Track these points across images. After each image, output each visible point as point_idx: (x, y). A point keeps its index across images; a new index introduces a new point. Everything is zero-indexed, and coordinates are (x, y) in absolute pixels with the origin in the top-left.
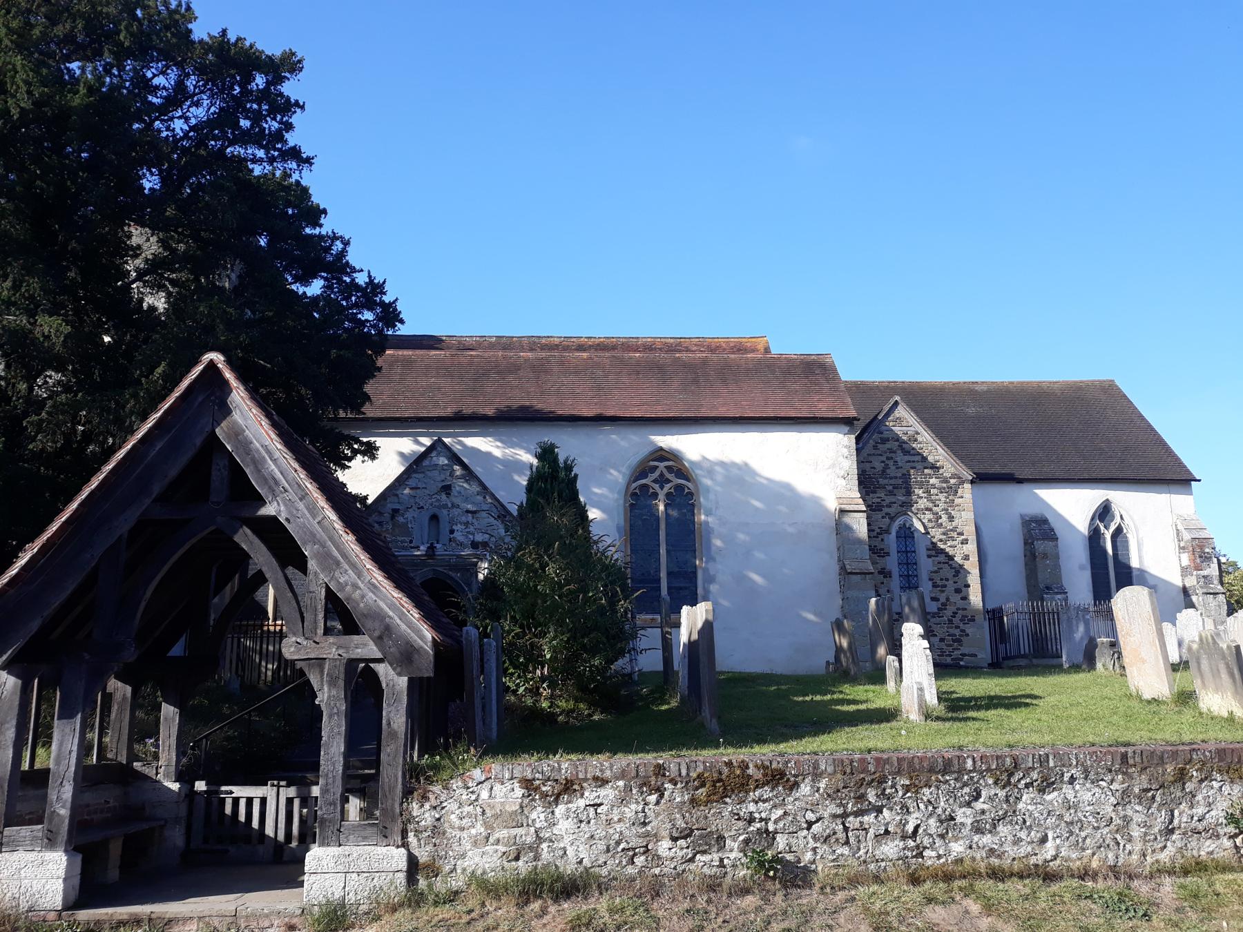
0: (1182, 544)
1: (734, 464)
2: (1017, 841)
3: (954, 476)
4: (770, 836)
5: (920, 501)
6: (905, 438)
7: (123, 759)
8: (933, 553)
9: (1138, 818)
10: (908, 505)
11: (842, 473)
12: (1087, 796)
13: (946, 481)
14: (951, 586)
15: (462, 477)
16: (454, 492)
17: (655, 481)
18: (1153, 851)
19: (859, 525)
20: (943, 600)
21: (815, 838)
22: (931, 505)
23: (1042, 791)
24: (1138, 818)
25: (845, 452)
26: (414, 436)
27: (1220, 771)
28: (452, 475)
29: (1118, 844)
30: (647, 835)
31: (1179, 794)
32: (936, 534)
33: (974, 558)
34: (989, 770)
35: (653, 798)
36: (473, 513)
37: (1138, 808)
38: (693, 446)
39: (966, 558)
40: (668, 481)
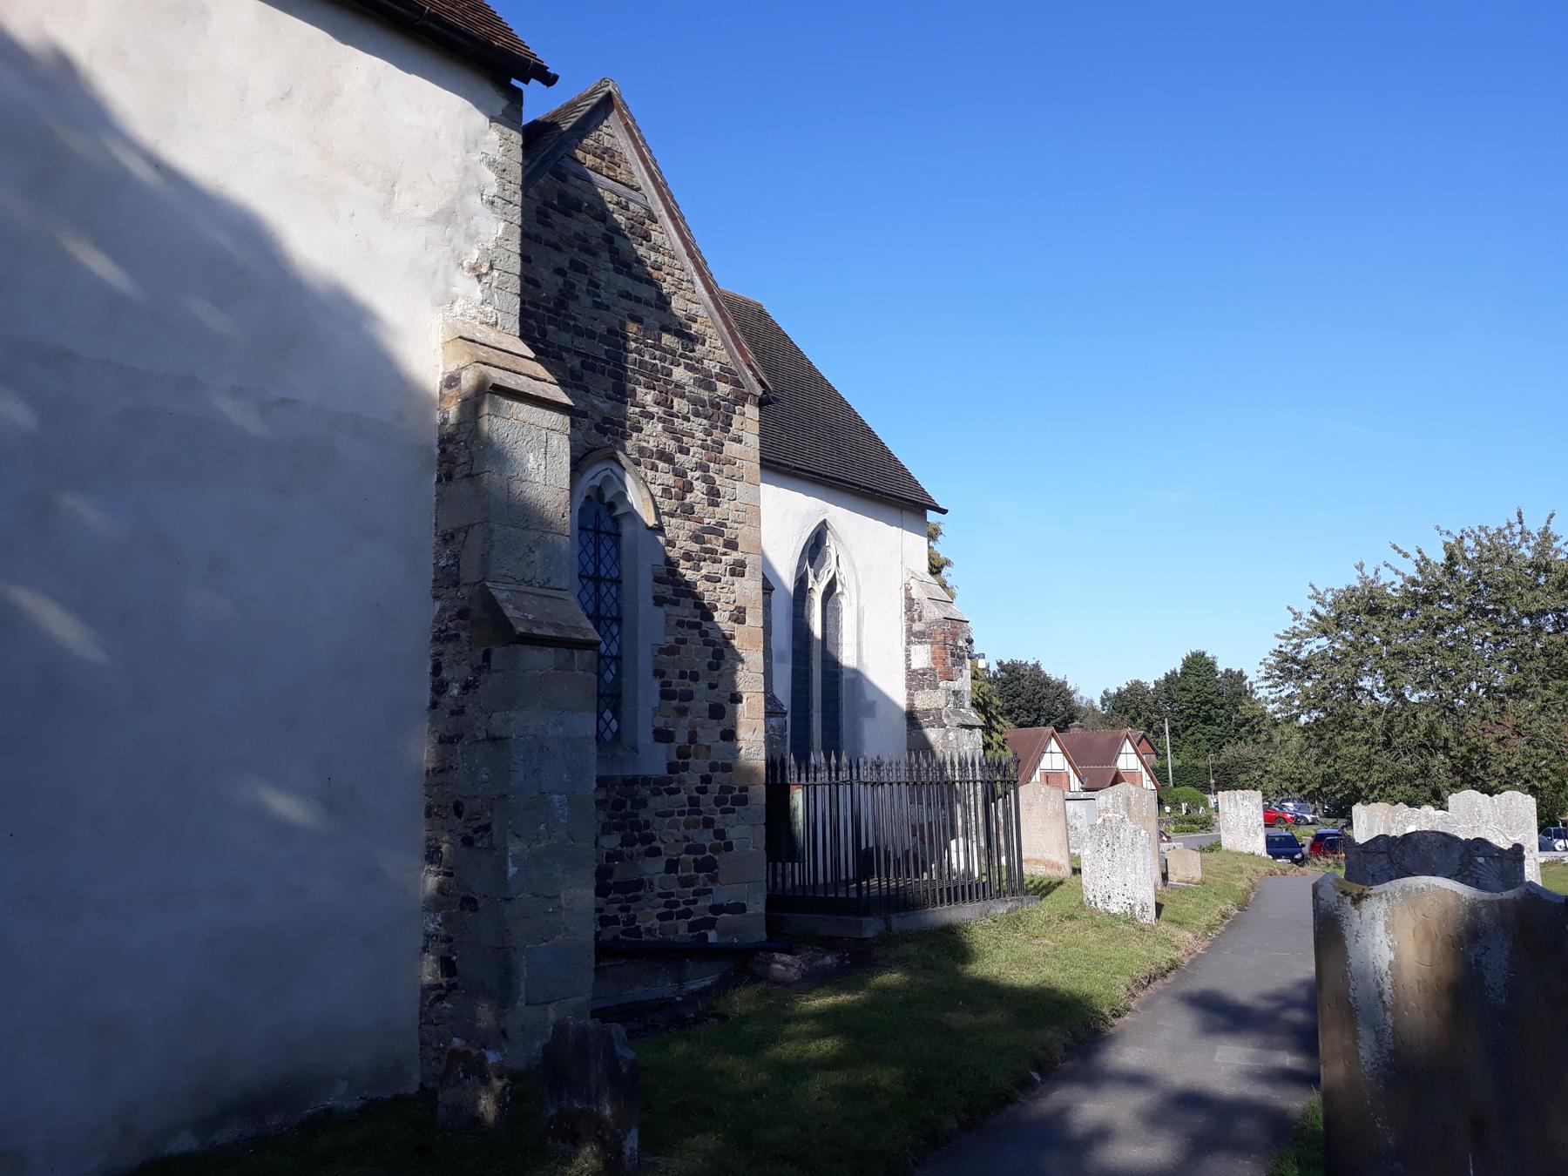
0: (917, 627)
3: (727, 374)
6: (620, 219)
8: (667, 590)
14: (700, 705)
20: (682, 739)
22: (671, 446)
32: (679, 533)
33: (754, 620)
39: (739, 616)
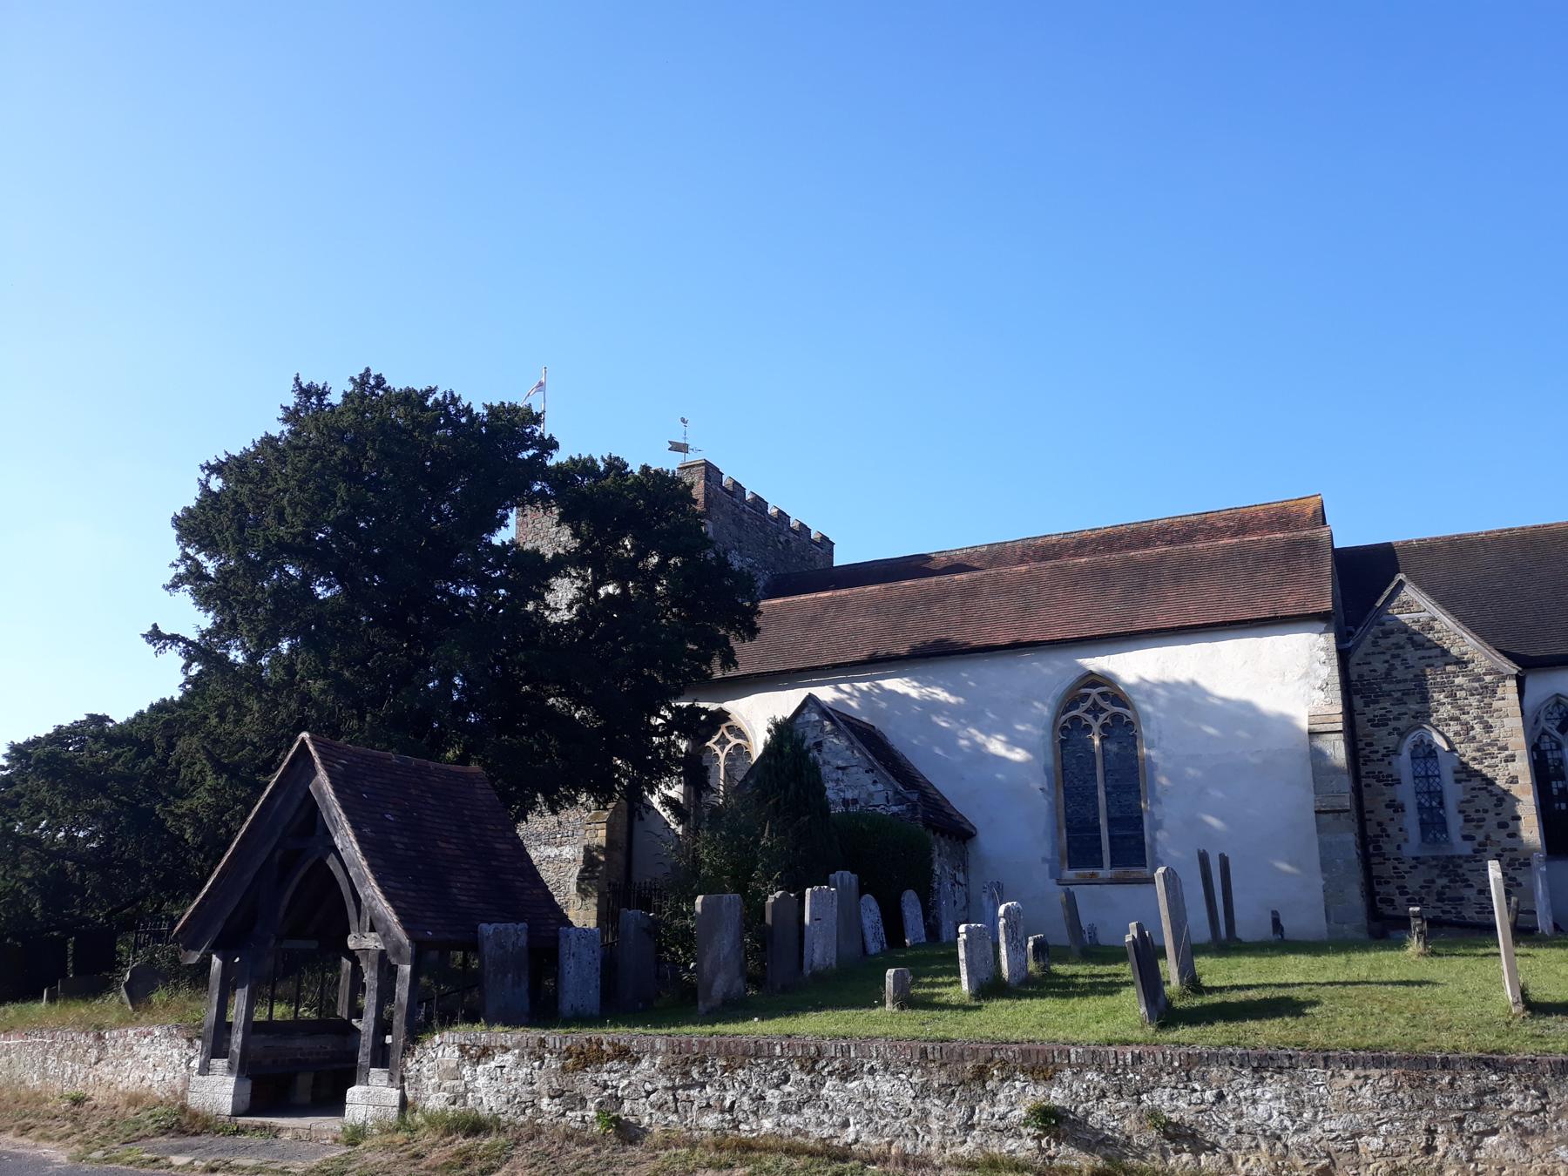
1: (1178, 684)
2: (820, 1123)
4: (619, 1101)
5: (1442, 709)
6: (1416, 627)
7: (345, 1017)
8: (1464, 776)
9: (936, 1111)
10: (1424, 715)
11: (1319, 683)
12: (886, 1087)
13: (1478, 679)
14: (1491, 821)
15: (832, 732)
16: (825, 749)
17: (1087, 711)
18: (953, 1145)
19: (1336, 750)
20: (1480, 837)
21: (651, 1105)
23: (844, 1079)
24: (936, 1111)
25: (1322, 656)
26: (835, 683)
27: (1023, 1071)
28: (822, 730)
29: (917, 1134)
30: (533, 1092)
31: (980, 1091)
32: (1467, 751)
34: (795, 1056)
35: (536, 1064)
36: (843, 769)
37: (937, 1102)
38: (1130, 666)
39: (1514, 780)
40: (1103, 710)
